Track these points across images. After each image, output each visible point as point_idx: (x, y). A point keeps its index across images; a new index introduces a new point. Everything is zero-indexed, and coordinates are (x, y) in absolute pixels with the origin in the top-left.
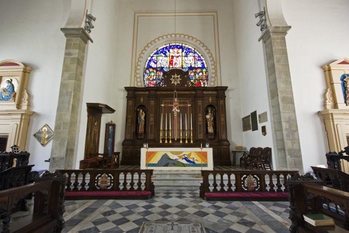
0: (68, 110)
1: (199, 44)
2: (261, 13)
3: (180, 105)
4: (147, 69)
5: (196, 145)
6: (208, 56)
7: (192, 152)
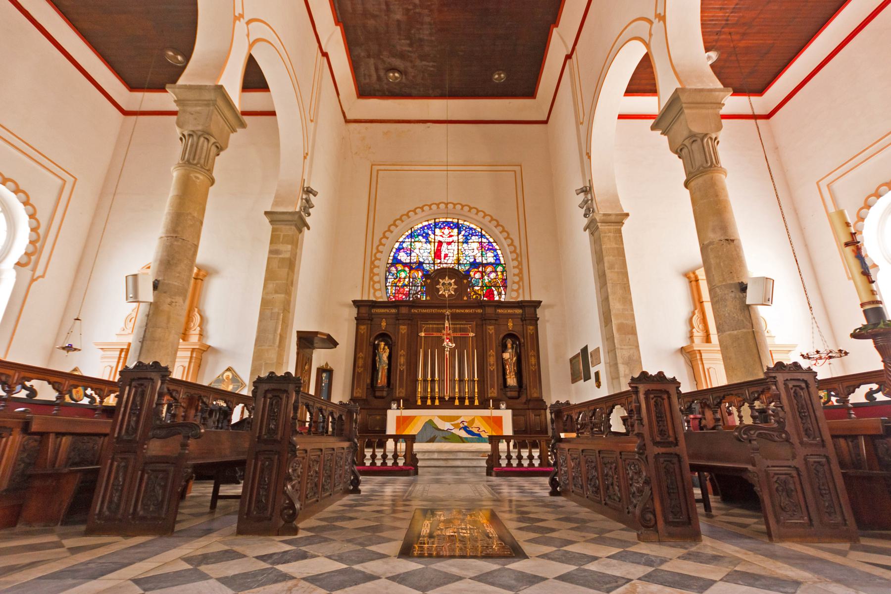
0: (274, 343)
1: (490, 222)
2: (584, 189)
4: (393, 265)
5: (484, 405)
6: (505, 243)
7: (474, 416)
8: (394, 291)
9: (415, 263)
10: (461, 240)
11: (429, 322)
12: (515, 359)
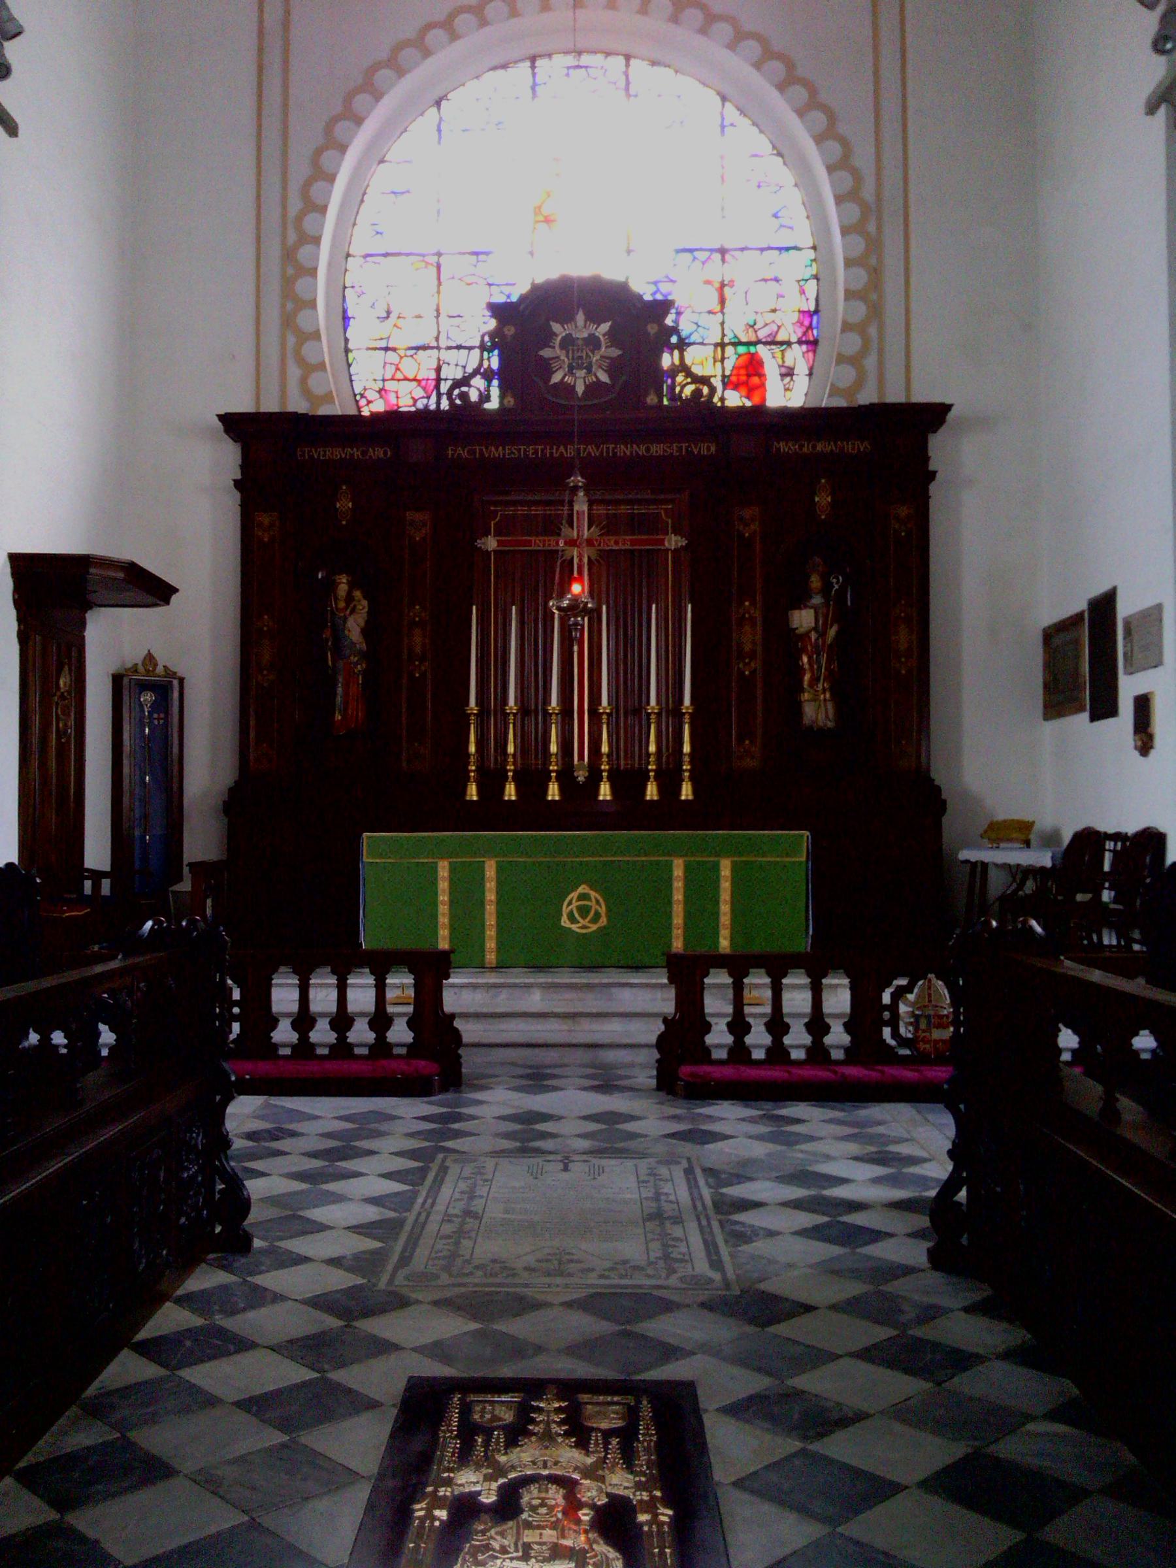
3: (611, 544)
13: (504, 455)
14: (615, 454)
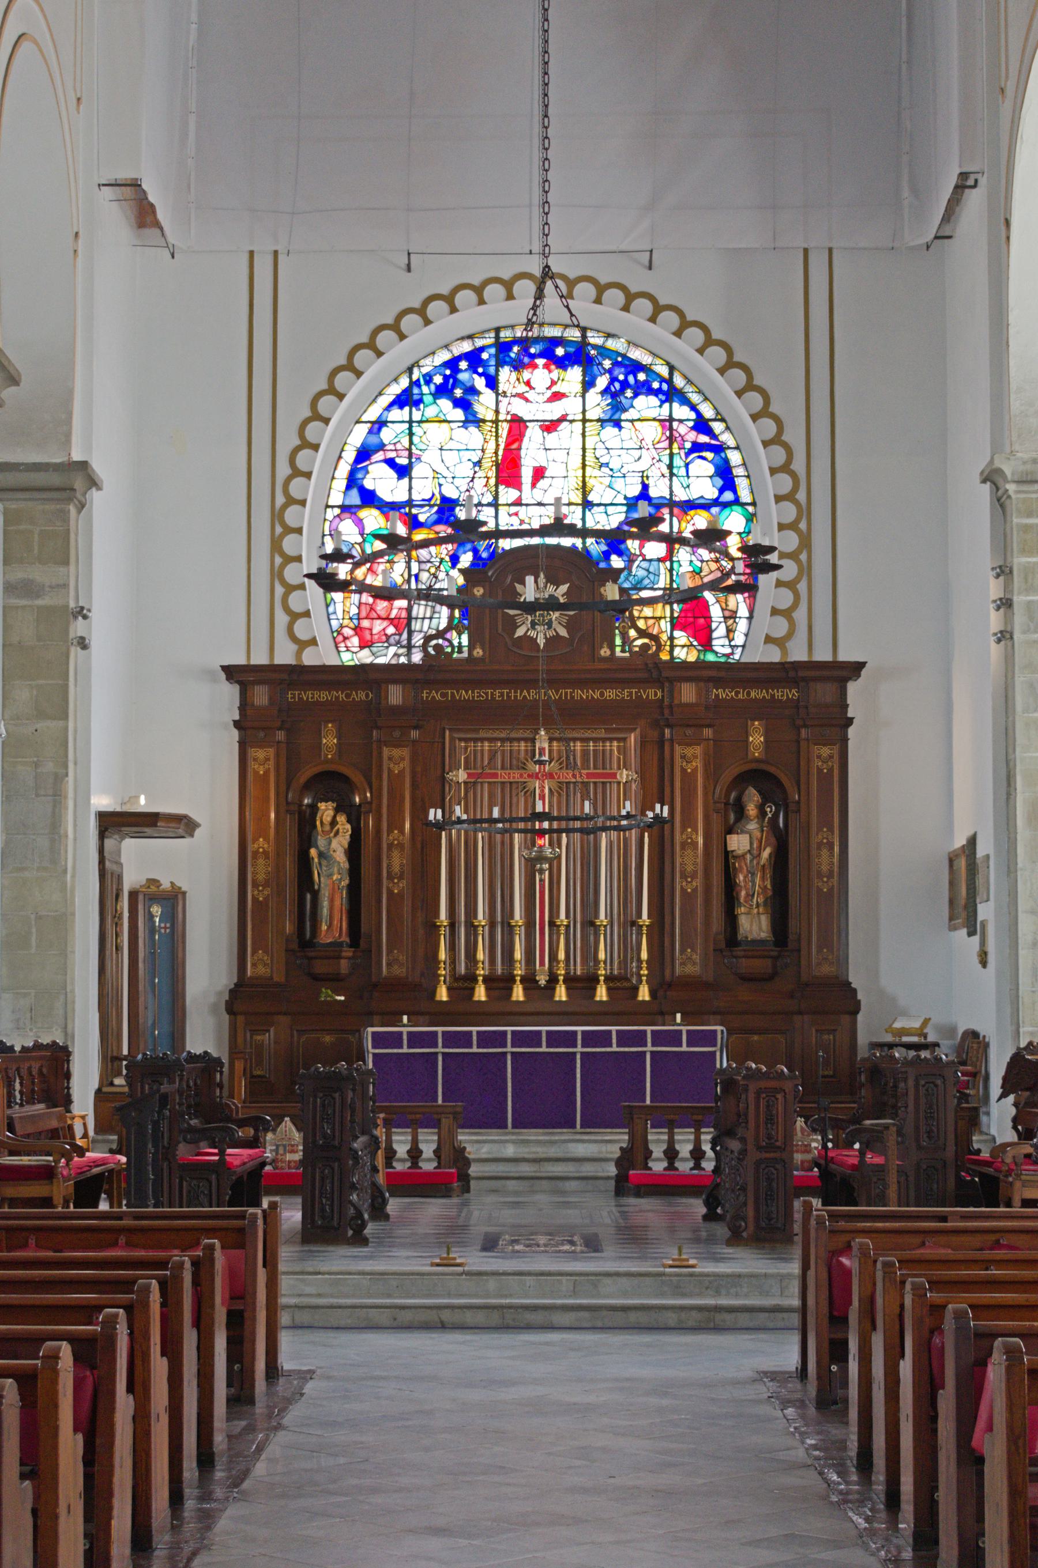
8: (354, 610)
9: (428, 502)
10: (593, 414)
11: (482, 734)
12: (766, 853)
13: (473, 697)
14: (572, 697)
